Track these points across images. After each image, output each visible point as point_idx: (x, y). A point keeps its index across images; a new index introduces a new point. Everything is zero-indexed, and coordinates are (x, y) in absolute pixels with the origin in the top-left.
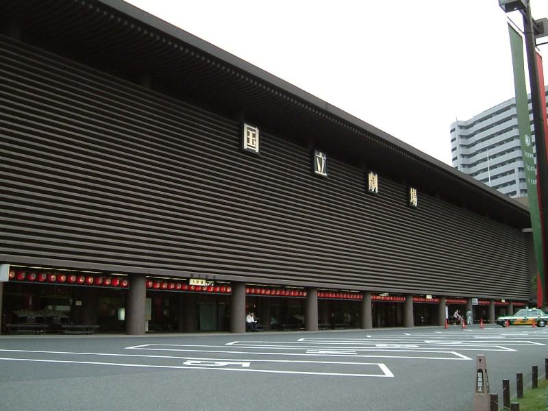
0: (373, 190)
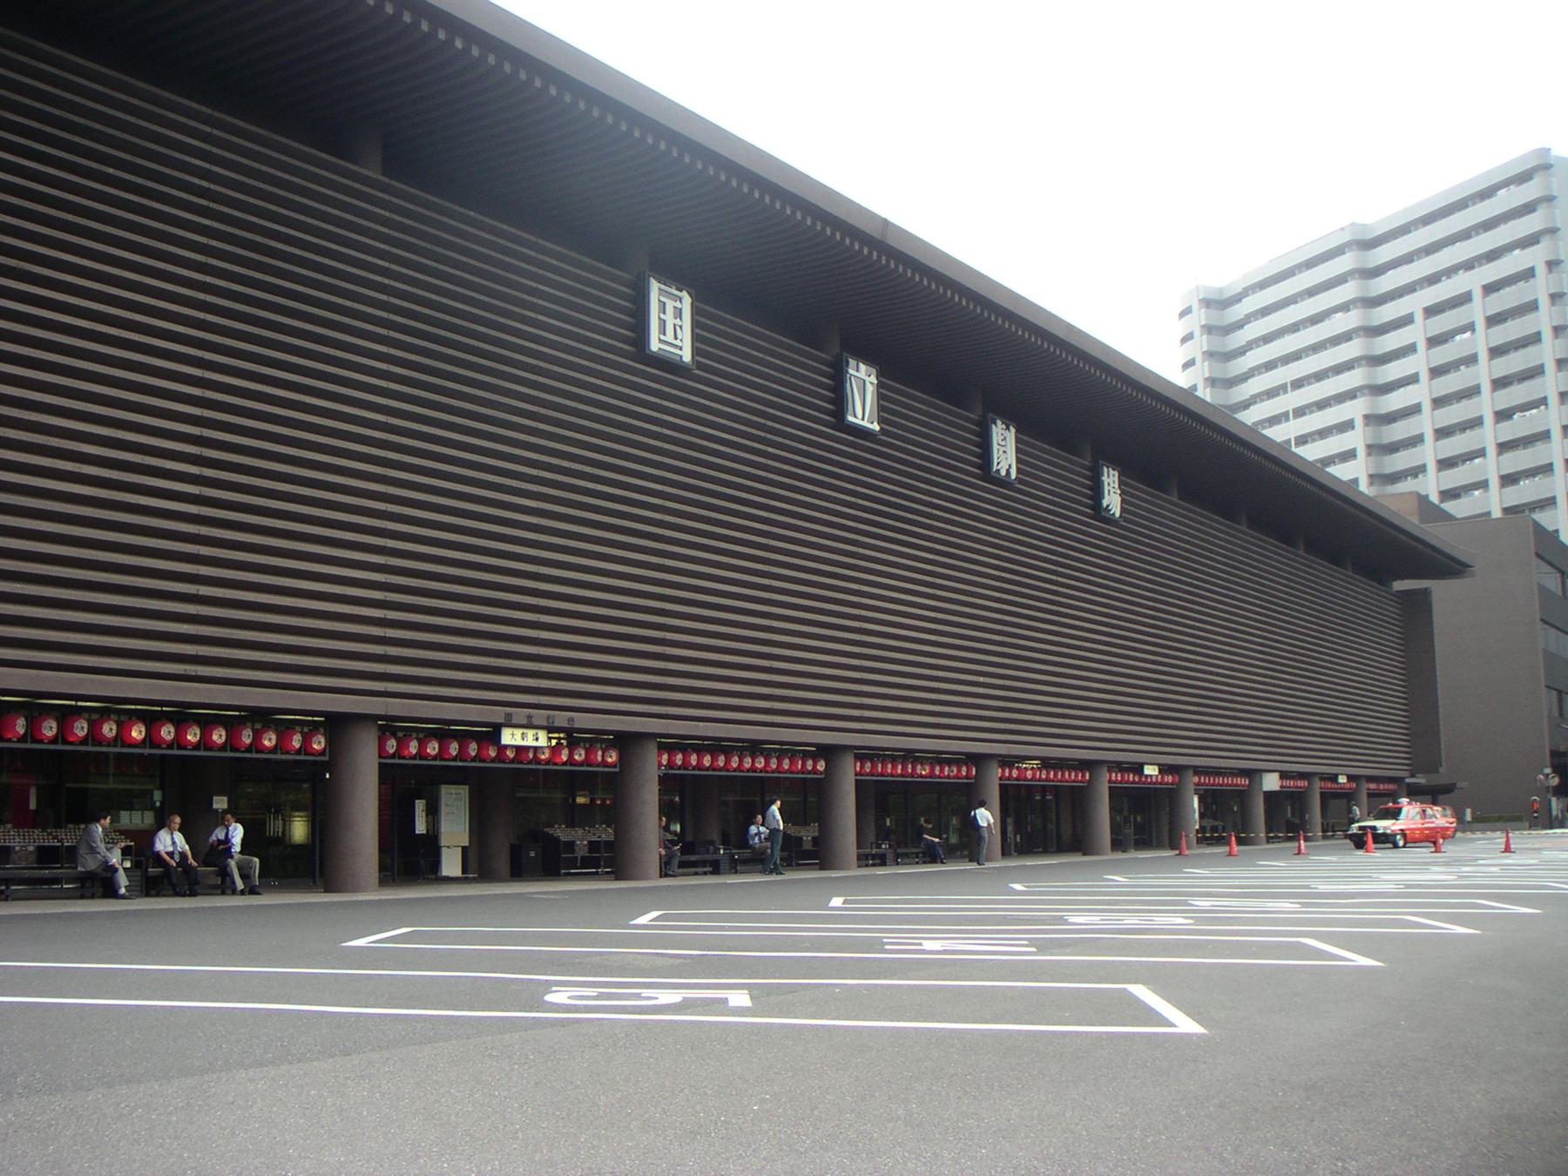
0: (1003, 473)
